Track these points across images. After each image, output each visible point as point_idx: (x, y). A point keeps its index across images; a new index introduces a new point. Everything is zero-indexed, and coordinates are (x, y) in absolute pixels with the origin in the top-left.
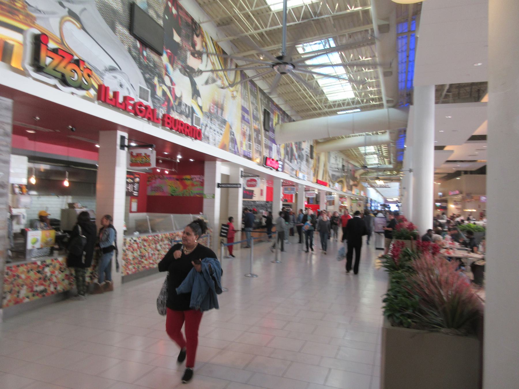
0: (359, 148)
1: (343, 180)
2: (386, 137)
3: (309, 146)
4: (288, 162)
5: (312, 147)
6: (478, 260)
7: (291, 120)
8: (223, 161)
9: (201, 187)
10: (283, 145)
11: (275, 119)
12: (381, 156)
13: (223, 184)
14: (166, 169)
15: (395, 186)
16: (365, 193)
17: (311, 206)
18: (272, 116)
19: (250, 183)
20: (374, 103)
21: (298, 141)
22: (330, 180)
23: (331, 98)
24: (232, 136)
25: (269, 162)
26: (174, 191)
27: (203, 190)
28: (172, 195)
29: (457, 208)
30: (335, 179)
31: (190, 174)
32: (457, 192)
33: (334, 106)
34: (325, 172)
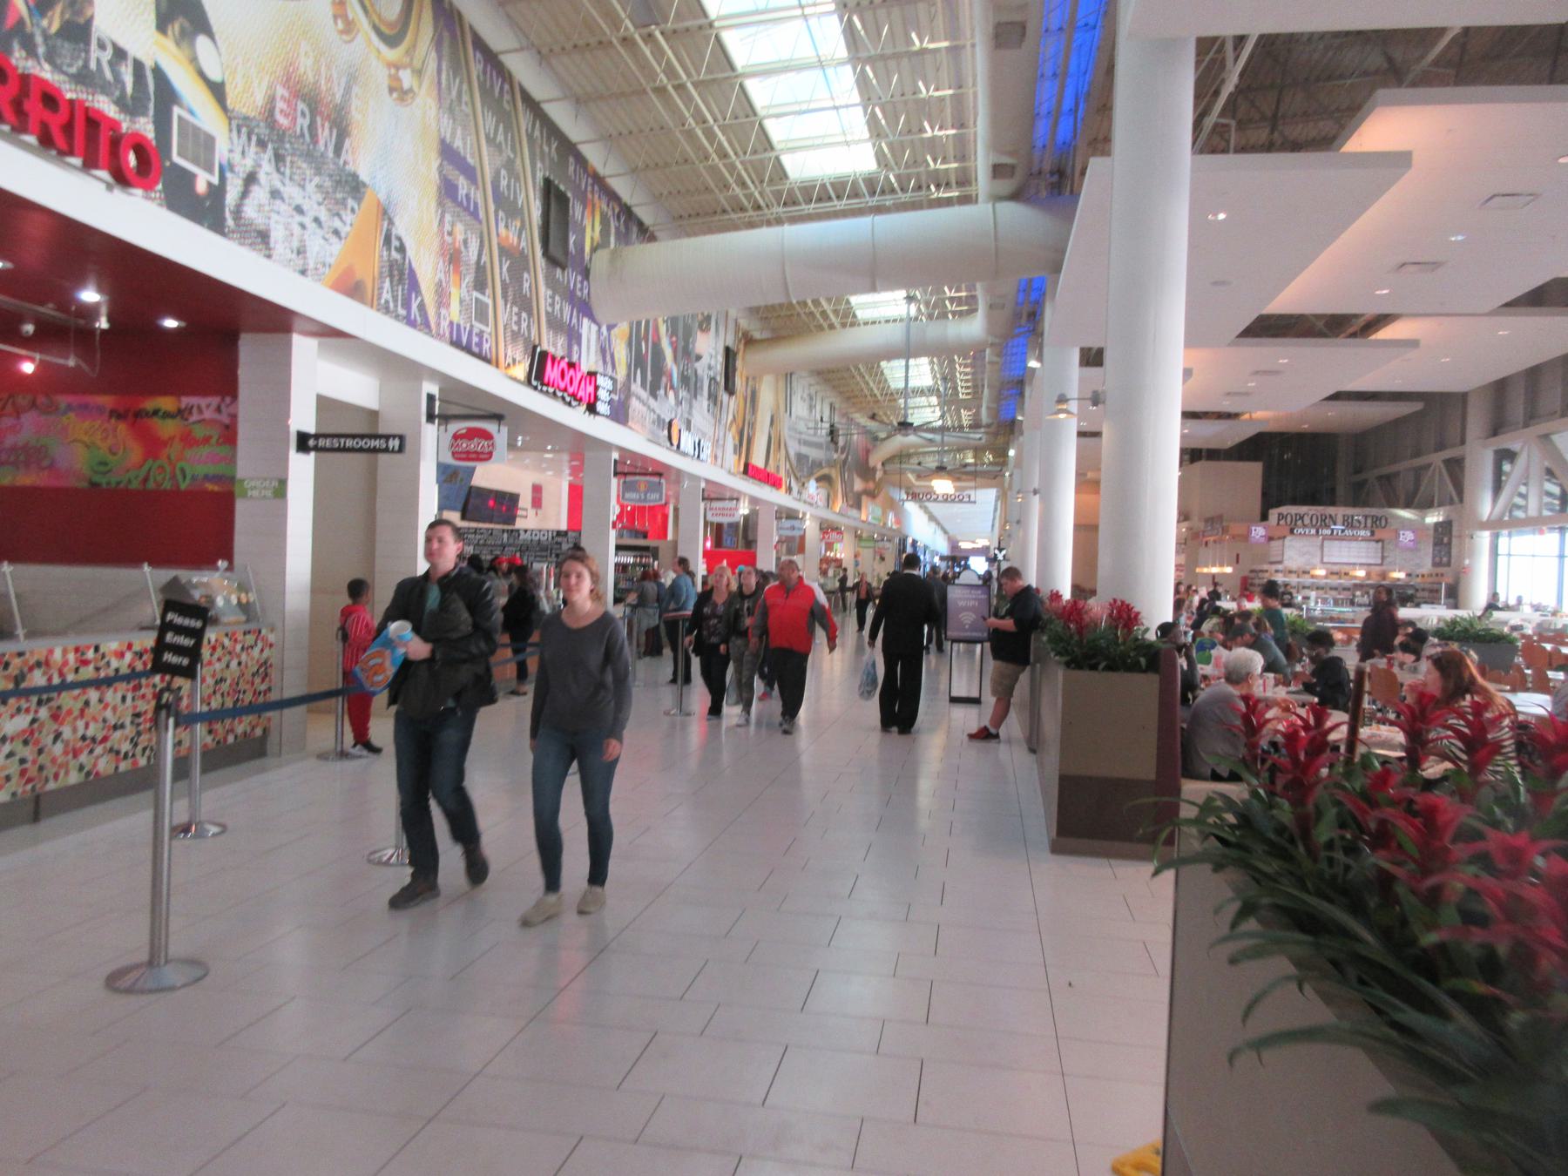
0: (883, 364)
1: (834, 473)
2: (974, 328)
4: (644, 395)
5: (729, 354)
7: (646, 234)
8: (328, 333)
9: (223, 450)
10: (623, 328)
11: (589, 227)
12: (949, 401)
13: (326, 436)
14: (23, 352)
15: (987, 497)
16: (898, 521)
17: (728, 556)
18: (576, 210)
19: (465, 445)
22: (792, 472)
24: (395, 255)
25: (552, 373)
26: (102, 468)
27: (232, 460)
28: (94, 485)
30: (805, 468)
31: (177, 390)
34: (774, 443)
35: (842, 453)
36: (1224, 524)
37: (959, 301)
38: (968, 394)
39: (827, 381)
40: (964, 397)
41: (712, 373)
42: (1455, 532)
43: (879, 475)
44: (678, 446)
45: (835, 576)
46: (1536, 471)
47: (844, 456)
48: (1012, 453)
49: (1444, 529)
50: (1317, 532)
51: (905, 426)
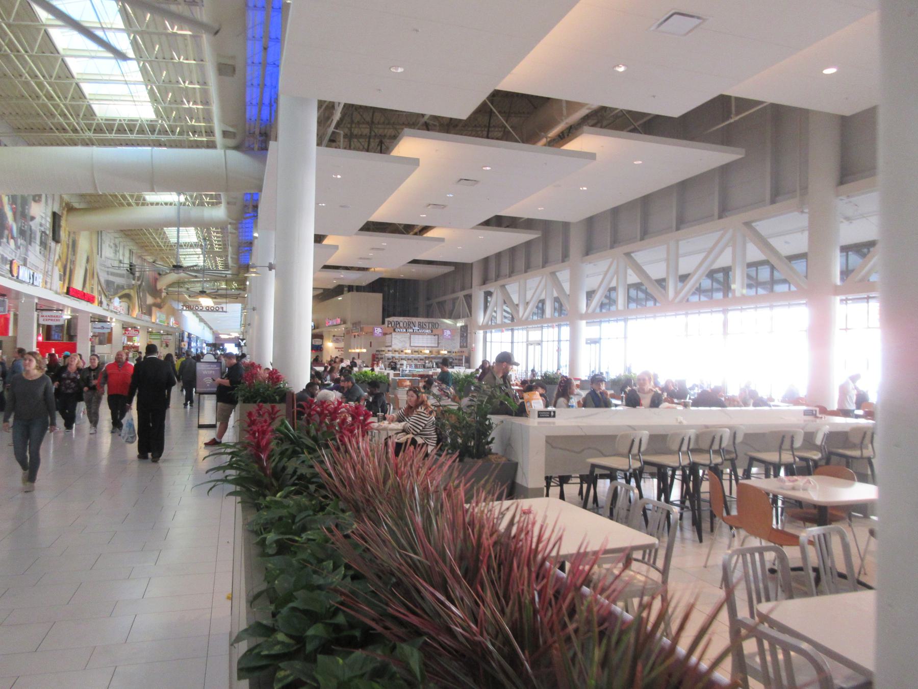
1: (133, 293)
2: (220, 213)
3: (50, 214)
5: (55, 217)
6: (397, 433)
12: (208, 252)
15: (235, 309)
16: (177, 322)
20: (197, 138)
21: (19, 192)
22: (103, 292)
23: (103, 111)
29: (336, 348)
30: (110, 290)
32: (339, 321)
33: (110, 128)
35: (138, 280)
36: (362, 326)
37: (211, 197)
38: (219, 248)
39: (127, 235)
40: (217, 250)
41: (43, 229)
42: (469, 331)
43: (164, 294)
44: (17, 277)
45: (133, 357)
46: (500, 301)
47: (139, 283)
48: (248, 283)
49: (464, 329)
50: (406, 330)
51: (178, 267)
